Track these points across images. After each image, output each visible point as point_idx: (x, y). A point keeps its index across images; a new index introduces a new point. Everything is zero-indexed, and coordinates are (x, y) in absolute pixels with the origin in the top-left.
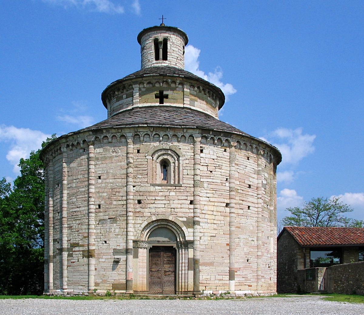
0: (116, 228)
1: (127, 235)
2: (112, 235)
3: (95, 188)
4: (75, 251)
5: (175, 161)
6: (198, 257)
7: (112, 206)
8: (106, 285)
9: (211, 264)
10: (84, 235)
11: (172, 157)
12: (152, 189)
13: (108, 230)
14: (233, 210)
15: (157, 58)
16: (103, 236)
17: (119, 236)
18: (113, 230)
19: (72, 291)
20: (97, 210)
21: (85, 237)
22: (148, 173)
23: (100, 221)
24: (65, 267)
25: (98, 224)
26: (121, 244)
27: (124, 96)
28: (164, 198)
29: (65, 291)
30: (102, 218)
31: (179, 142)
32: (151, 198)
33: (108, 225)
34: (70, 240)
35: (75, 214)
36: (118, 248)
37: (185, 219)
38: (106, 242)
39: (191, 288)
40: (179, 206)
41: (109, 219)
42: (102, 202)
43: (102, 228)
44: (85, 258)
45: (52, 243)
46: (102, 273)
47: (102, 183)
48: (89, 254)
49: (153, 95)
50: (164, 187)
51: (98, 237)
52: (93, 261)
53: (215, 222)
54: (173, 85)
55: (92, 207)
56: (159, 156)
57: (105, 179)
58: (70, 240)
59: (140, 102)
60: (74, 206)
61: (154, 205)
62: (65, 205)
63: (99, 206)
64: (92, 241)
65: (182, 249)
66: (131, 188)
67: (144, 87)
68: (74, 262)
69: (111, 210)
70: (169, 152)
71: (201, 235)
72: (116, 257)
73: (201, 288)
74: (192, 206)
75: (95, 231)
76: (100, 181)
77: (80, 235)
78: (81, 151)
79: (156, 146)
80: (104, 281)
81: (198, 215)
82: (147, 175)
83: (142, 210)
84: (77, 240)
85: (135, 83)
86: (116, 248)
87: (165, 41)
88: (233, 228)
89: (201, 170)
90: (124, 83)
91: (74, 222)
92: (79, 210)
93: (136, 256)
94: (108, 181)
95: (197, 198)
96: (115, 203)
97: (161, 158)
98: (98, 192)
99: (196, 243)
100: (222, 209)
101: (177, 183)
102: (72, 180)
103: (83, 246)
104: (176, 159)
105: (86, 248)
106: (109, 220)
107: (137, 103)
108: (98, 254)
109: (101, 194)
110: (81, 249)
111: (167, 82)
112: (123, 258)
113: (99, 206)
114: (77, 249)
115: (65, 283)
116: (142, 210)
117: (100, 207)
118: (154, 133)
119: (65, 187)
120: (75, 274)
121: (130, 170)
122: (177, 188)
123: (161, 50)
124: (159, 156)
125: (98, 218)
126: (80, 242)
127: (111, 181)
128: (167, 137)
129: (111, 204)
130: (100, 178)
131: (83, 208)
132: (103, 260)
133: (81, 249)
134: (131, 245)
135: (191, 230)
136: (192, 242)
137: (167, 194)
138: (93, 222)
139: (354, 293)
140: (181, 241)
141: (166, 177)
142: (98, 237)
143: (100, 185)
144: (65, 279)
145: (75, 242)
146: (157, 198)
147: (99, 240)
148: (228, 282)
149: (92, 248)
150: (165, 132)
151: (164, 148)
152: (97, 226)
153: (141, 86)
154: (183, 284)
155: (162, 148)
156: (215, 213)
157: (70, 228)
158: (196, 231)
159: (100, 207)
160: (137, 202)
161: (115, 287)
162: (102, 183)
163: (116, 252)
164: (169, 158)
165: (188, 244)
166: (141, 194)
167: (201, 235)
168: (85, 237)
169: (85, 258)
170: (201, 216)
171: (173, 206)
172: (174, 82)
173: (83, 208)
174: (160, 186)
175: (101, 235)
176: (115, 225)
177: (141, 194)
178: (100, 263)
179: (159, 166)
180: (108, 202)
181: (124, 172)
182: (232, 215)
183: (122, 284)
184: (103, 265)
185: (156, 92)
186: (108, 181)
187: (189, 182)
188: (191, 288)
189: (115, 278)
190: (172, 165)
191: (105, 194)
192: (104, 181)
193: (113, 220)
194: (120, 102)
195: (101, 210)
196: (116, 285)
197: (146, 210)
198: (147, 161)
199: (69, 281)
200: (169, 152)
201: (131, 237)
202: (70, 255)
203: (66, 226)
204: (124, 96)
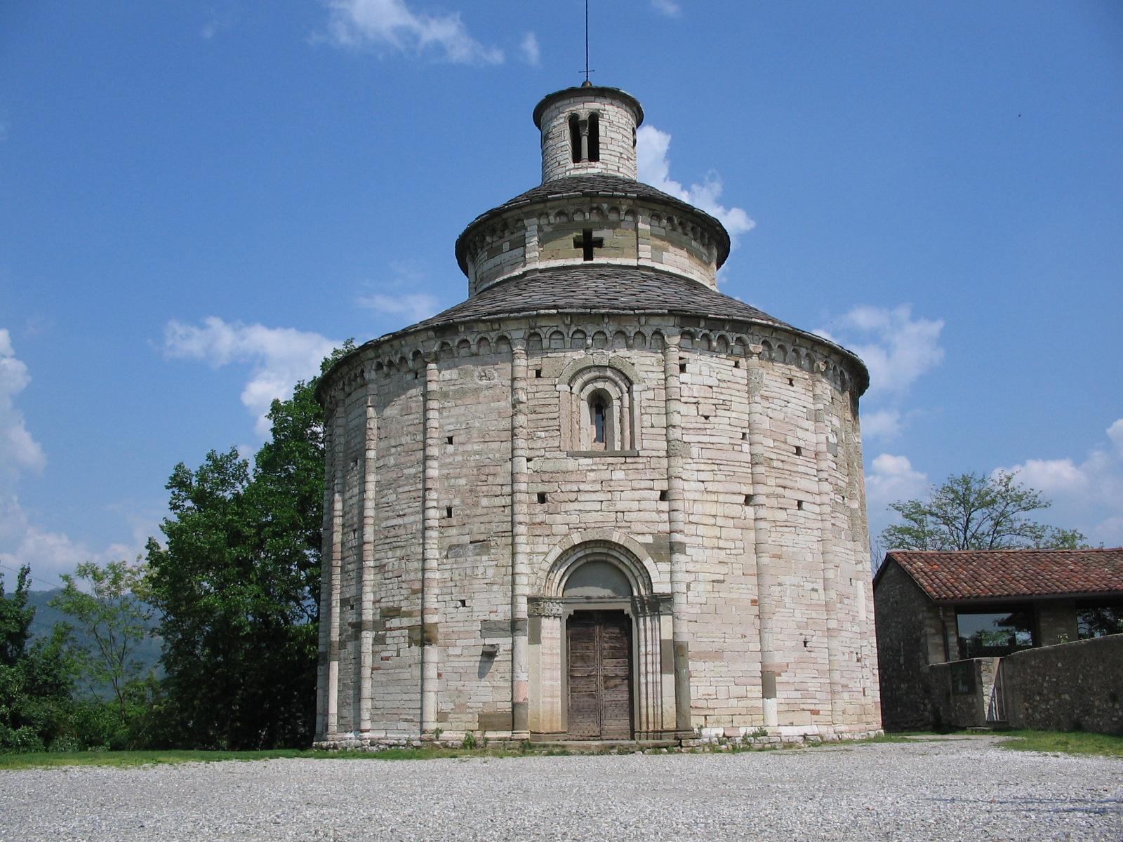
0: (487, 566)
1: (513, 583)
2: (478, 584)
3: (441, 466)
4: (391, 629)
5: (622, 393)
6: (684, 637)
7: (479, 511)
8: (464, 717)
9: (716, 655)
10: (413, 587)
11: (616, 384)
12: (571, 464)
13: (469, 572)
14: (762, 513)
15: (577, 157)
16: (458, 589)
17: (495, 588)
18: (480, 571)
19: (383, 735)
20: (444, 523)
21: (414, 592)
22: (562, 426)
23: (450, 548)
24: (366, 672)
25: (447, 557)
26: (500, 608)
27: (506, 246)
28: (598, 487)
29: (366, 735)
30: (455, 541)
31: (629, 347)
32: (569, 487)
33: (470, 559)
34: (379, 601)
35: (393, 533)
36: (493, 617)
37: (649, 539)
38: (463, 603)
39: (670, 724)
40: (635, 506)
41: (471, 542)
42: (456, 502)
43: (455, 566)
44: (413, 647)
45: (336, 610)
46: (454, 684)
47: (455, 454)
48: (423, 636)
49: (569, 240)
50: (598, 459)
51: (445, 590)
52: (433, 653)
53: (722, 544)
54: (613, 217)
55: (432, 513)
56: (586, 384)
57: (463, 444)
58: (379, 601)
59: (540, 258)
60: (391, 514)
61: (576, 506)
62: (370, 512)
63: (449, 511)
64: (432, 602)
65: (645, 617)
66: (522, 465)
67: (549, 224)
68: (387, 659)
69: (475, 520)
70: (609, 373)
71: (690, 578)
72: (489, 641)
73: (695, 721)
74: (664, 506)
75: (438, 575)
76: (450, 448)
77: (404, 585)
78: (410, 377)
79: (579, 359)
80: (460, 708)
81: (681, 526)
82: (559, 430)
83: (548, 519)
84: (396, 598)
85: (530, 215)
86: (487, 618)
87: (594, 118)
88: (765, 560)
89: (684, 414)
90: (504, 216)
91: (390, 554)
92: (401, 522)
93: (535, 639)
94: (469, 447)
95: (677, 484)
96: (485, 502)
97: (590, 388)
98: (447, 477)
99: (677, 599)
100: (737, 511)
101: (627, 447)
102: (388, 449)
103: (409, 614)
104: (625, 389)
105: (416, 621)
106: (471, 547)
107: (533, 260)
108: (446, 635)
109: (453, 480)
110: (406, 622)
111: (599, 210)
112: (504, 643)
113: (449, 511)
114: (395, 622)
115: (366, 715)
116: (548, 519)
117: (450, 515)
118: (574, 329)
119: (372, 465)
120: (391, 689)
121: (521, 420)
122: (629, 460)
123: (586, 138)
124: (586, 384)
125: (447, 543)
126: (403, 604)
127: (476, 447)
128: (602, 337)
129: (476, 505)
130: (450, 441)
131: (412, 518)
132: (457, 651)
133: (406, 622)
134: (523, 609)
135: (664, 566)
136: (668, 599)
137: (606, 475)
138: (433, 553)
139: (1077, 727)
140: (641, 597)
141: (602, 435)
142: (445, 590)
143: (451, 460)
144: (367, 704)
145: (392, 604)
146: (582, 487)
147: (448, 598)
148: (759, 703)
149: (431, 619)
150: (598, 325)
151: (596, 363)
152: (443, 563)
153: (543, 221)
154: (651, 710)
155: (592, 364)
156: (720, 521)
157: (380, 568)
158: (677, 567)
159: (450, 515)
160: (535, 498)
161: (487, 722)
162: (455, 454)
163: (488, 628)
164: (608, 386)
165: (659, 604)
166: (546, 477)
167: (690, 578)
168: (414, 592)
169: (413, 647)
170: (690, 529)
171: (620, 506)
172: (615, 209)
173: (412, 518)
174: (589, 457)
175: (453, 584)
176: (485, 558)
177: (546, 477)
178: (451, 659)
179: (585, 406)
180: (470, 501)
181: (506, 424)
182: (762, 524)
183: (502, 714)
184: (456, 664)
185: (575, 234)
186: (469, 447)
187: (655, 444)
188: (670, 724)
189: (485, 699)
190: (616, 403)
191: (463, 481)
192: (461, 449)
193: (482, 545)
194: (497, 260)
195: (454, 521)
196: (488, 716)
197: (559, 518)
198: (559, 397)
199: (375, 708)
200: (609, 373)
201: (524, 590)
202: (379, 640)
203: (372, 564)
204: (506, 246)
